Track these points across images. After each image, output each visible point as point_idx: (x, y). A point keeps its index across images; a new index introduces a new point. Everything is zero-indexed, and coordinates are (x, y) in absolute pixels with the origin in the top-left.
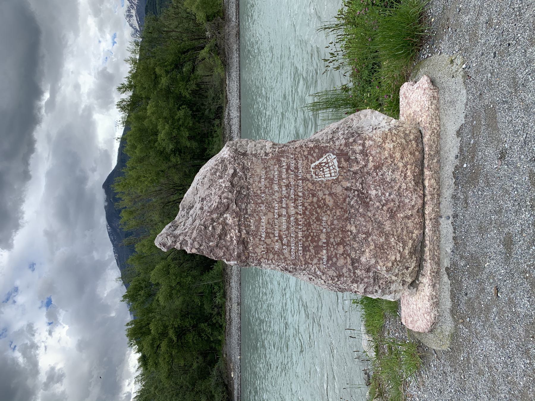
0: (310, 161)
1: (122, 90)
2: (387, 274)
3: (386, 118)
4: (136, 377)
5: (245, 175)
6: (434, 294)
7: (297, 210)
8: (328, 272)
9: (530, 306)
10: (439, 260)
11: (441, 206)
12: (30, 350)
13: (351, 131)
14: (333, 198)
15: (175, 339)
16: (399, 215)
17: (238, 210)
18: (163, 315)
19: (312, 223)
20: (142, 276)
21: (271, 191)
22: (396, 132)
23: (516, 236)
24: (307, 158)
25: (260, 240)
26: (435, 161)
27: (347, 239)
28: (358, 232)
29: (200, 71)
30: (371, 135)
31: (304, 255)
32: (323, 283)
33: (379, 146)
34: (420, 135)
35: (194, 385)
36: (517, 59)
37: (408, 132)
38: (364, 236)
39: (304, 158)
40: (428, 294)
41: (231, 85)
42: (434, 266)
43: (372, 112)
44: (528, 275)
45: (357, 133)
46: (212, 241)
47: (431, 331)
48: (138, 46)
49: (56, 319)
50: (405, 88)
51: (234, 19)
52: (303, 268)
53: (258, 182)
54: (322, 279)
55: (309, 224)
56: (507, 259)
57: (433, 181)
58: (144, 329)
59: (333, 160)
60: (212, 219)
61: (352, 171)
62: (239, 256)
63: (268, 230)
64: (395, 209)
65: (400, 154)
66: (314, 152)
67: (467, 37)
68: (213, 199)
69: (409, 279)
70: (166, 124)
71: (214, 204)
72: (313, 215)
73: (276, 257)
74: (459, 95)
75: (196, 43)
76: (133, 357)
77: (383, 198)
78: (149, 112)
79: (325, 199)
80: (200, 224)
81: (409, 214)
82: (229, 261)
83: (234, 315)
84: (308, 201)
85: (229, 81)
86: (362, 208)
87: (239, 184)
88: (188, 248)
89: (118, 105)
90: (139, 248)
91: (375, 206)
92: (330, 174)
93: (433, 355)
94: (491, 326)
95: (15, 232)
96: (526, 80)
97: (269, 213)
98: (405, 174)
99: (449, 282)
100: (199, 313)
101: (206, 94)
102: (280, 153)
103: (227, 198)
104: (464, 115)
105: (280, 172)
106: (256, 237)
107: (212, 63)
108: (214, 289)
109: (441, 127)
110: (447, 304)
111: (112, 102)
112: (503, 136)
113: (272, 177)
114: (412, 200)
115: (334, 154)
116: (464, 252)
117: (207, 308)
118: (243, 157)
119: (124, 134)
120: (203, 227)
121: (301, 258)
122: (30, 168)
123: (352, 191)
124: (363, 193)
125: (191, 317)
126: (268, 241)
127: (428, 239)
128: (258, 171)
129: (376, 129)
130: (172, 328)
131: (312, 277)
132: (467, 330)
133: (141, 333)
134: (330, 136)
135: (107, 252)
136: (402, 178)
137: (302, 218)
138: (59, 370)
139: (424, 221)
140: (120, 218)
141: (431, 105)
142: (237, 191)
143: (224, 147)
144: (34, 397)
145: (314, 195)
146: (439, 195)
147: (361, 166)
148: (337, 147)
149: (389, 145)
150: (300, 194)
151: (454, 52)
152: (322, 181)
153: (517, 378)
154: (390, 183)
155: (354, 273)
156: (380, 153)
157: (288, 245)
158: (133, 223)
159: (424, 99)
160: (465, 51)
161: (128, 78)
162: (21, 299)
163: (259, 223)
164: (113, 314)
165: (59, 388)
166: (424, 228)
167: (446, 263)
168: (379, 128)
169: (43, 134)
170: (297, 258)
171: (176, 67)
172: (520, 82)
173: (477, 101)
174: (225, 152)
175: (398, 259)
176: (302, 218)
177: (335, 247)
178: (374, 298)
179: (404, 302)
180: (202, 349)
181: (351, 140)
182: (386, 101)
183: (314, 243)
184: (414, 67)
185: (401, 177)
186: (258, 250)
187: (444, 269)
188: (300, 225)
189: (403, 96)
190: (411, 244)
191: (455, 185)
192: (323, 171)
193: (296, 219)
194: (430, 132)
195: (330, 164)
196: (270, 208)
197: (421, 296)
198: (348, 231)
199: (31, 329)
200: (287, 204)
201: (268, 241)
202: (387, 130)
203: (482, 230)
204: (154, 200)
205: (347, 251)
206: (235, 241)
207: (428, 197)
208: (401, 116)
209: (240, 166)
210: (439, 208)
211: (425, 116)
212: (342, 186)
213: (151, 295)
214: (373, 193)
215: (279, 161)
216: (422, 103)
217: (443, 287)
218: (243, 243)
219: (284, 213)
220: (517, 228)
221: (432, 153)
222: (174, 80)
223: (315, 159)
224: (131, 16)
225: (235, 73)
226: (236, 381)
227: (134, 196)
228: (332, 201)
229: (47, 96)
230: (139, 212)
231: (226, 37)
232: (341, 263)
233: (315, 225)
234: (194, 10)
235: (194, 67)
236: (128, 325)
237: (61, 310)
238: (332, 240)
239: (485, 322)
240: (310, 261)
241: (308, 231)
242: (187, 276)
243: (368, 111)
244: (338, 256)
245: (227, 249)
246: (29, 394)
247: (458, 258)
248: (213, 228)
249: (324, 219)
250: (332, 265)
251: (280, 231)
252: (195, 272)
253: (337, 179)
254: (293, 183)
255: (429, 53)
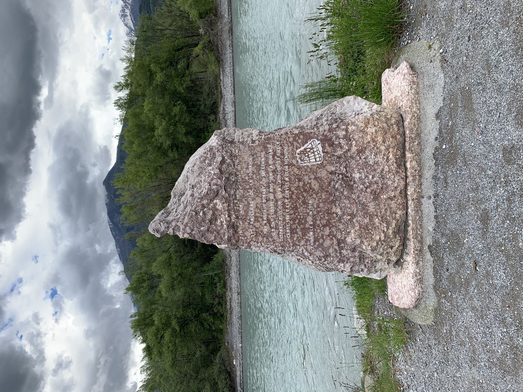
0: (295, 147)
1: (119, 88)
2: (372, 253)
3: (368, 104)
4: (142, 367)
5: (233, 162)
6: (418, 271)
7: (283, 194)
8: (315, 253)
9: (506, 277)
10: (422, 238)
11: (423, 187)
12: (36, 338)
13: (335, 117)
14: (318, 182)
15: (178, 328)
16: (382, 197)
17: (227, 195)
18: (165, 307)
19: (298, 207)
20: (144, 268)
21: (258, 177)
22: (377, 117)
23: (492, 212)
24: (292, 144)
25: (249, 224)
26: (416, 144)
27: (333, 221)
28: (344, 214)
29: (195, 68)
30: (353, 120)
31: (292, 238)
32: (311, 263)
33: (362, 131)
34: (401, 119)
35: (197, 373)
36: (490, 41)
37: (389, 117)
38: (349, 217)
39: (290, 145)
40: (412, 272)
41: (225, 80)
42: (418, 245)
43: (355, 98)
44: (503, 248)
45: (340, 119)
46: (203, 226)
47: (416, 307)
48: (133, 45)
49: (61, 309)
50: (387, 74)
51: (226, 16)
52: (291, 249)
53: (246, 169)
54: (309, 260)
55: (296, 208)
56: (484, 234)
57: (414, 163)
58: (148, 321)
59: (317, 145)
60: (203, 205)
61: (336, 156)
62: (229, 240)
63: (257, 214)
64: (378, 191)
65: (382, 138)
66: (299, 138)
67: (443, 23)
68: (203, 186)
69: (394, 258)
70: (163, 120)
71: (204, 191)
72: (299, 198)
73: (265, 239)
74: (438, 79)
75: (190, 40)
76: (138, 348)
77: (366, 181)
78: (146, 108)
79: (310, 183)
80: (191, 210)
81: (392, 196)
82: (220, 244)
83: (235, 305)
84: (295, 185)
85: (223, 77)
86: (346, 191)
87: (228, 171)
88: (180, 233)
89: (115, 103)
90: (140, 243)
91: (359, 189)
92: (315, 159)
93: (418, 329)
94: (471, 298)
95: (17, 223)
96: (498, 62)
97: (257, 198)
98: (388, 157)
99: (432, 259)
100: (200, 303)
101: (200, 90)
102: (266, 141)
103: (217, 185)
104: (442, 98)
105: (267, 159)
106: (246, 221)
107: (206, 60)
108: (214, 280)
109: (421, 110)
110: (430, 280)
111: (109, 98)
112: (478, 116)
113: (259, 163)
114: (395, 181)
115: (318, 140)
116: (445, 229)
117: (208, 297)
118: (231, 145)
119: (122, 131)
120: (194, 213)
121: (289, 240)
122: (32, 162)
123: (337, 175)
124: (347, 177)
125: (193, 308)
126: (257, 225)
127: (411, 218)
128: (246, 157)
129: (358, 114)
130: (175, 318)
131: (300, 258)
132: (449, 304)
133: (145, 324)
134: (314, 123)
135: (109, 246)
136: (385, 160)
137: (289, 202)
138: (66, 357)
139: (407, 201)
140: (121, 213)
141: (411, 90)
142: (226, 178)
143: (213, 136)
144: (42, 382)
145: (300, 180)
146: (420, 176)
147: (345, 150)
148: (321, 133)
149: (371, 130)
150: (287, 179)
151: (432, 38)
152: (308, 166)
153: (495, 346)
154: (373, 166)
155: (341, 253)
156: (362, 137)
157: (277, 228)
158: (134, 218)
159: (404, 84)
160: (442, 36)
161: (124, 76)
162: (25, 289)
163: (248, 208)
164: (118, 306)
165: (66, 375)
166: (407, 208)
167: (429, 241)
168: (362, 113)
169: (44, 131)
170: (285, 240)
171: (171, 64)
172: (492, 64)
173: (454, 84)
174: (213, 141)
175: (383, 238)
176: (289, 202)
177: (322, 229)
178: (360, 276)
179: (390, 280)
180: (204, 338)
181: (334, 126)
182: (370, 88)
183: (301, 226)
184: (395, 54)
185: (383, 159)
186: (247, 234)
187: (427, 247)
188: (287, 208)
189: (385, 82)
190: (394, 224)
191: (436, 166)
192: (308, 156)
193: (284, 203)
194: (410, 116)
195: (315, 150)
196: (258, 193)
197: (406, 274)
198: (334, 213)
199: (36, 318)
200: (274, 189)
201: (257, 225)
202: (369, 115)
203: (461, 207)
204: (153, 195)
205: (333, 232)
206: (225, 226)
207: (410, 179)
208: (383, 101)
209: (228, 154)
210: (420, 188)
211: (405, 101)
212: (327, 170)
213: (153, 287)
214: (357, 176)
215: (265, 148)
216: (403, 88)
217: (426, 264)
218: (233, 227)
219: (271, 197)
220: (493, 204)
221: (413, 136)
222: (169, 77)
223: (300, 145)
224: (126, 16)
225: (229, 68)
226: (238, 368)
227: (133, 192)
228: (317, 185)
229: (44, 92)
230: (139, 207)
231: (219, 34)
232: (328, 244)
233: (302, 208)
234: (187, 8)
235: (188, 64)
236: (131, 317)
237: (66, 300)
238: (318, 222)
239: (465, 295)
240: (297, 243)
241: (295, 214)
242: (187, 267)
243: (351, 98)
244: (325, 237)
245: (218, 233)
246: (36, 381)
247: (439, 236)
248: (204, 213)
249: (310, 202)
250: (319, 246)
251: (269, 214)
252: (195, 264)
253: (322, 164)
254: (279, 168)
255: (409, 40)
